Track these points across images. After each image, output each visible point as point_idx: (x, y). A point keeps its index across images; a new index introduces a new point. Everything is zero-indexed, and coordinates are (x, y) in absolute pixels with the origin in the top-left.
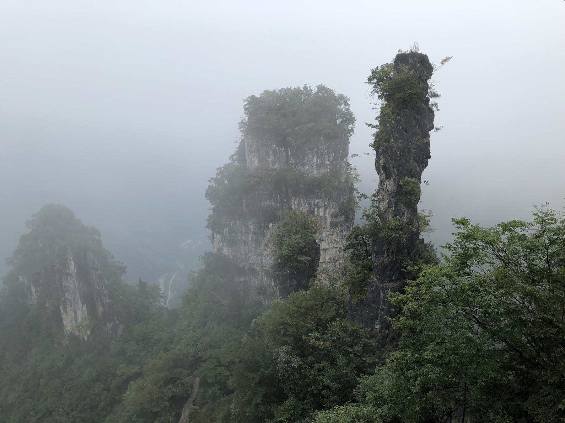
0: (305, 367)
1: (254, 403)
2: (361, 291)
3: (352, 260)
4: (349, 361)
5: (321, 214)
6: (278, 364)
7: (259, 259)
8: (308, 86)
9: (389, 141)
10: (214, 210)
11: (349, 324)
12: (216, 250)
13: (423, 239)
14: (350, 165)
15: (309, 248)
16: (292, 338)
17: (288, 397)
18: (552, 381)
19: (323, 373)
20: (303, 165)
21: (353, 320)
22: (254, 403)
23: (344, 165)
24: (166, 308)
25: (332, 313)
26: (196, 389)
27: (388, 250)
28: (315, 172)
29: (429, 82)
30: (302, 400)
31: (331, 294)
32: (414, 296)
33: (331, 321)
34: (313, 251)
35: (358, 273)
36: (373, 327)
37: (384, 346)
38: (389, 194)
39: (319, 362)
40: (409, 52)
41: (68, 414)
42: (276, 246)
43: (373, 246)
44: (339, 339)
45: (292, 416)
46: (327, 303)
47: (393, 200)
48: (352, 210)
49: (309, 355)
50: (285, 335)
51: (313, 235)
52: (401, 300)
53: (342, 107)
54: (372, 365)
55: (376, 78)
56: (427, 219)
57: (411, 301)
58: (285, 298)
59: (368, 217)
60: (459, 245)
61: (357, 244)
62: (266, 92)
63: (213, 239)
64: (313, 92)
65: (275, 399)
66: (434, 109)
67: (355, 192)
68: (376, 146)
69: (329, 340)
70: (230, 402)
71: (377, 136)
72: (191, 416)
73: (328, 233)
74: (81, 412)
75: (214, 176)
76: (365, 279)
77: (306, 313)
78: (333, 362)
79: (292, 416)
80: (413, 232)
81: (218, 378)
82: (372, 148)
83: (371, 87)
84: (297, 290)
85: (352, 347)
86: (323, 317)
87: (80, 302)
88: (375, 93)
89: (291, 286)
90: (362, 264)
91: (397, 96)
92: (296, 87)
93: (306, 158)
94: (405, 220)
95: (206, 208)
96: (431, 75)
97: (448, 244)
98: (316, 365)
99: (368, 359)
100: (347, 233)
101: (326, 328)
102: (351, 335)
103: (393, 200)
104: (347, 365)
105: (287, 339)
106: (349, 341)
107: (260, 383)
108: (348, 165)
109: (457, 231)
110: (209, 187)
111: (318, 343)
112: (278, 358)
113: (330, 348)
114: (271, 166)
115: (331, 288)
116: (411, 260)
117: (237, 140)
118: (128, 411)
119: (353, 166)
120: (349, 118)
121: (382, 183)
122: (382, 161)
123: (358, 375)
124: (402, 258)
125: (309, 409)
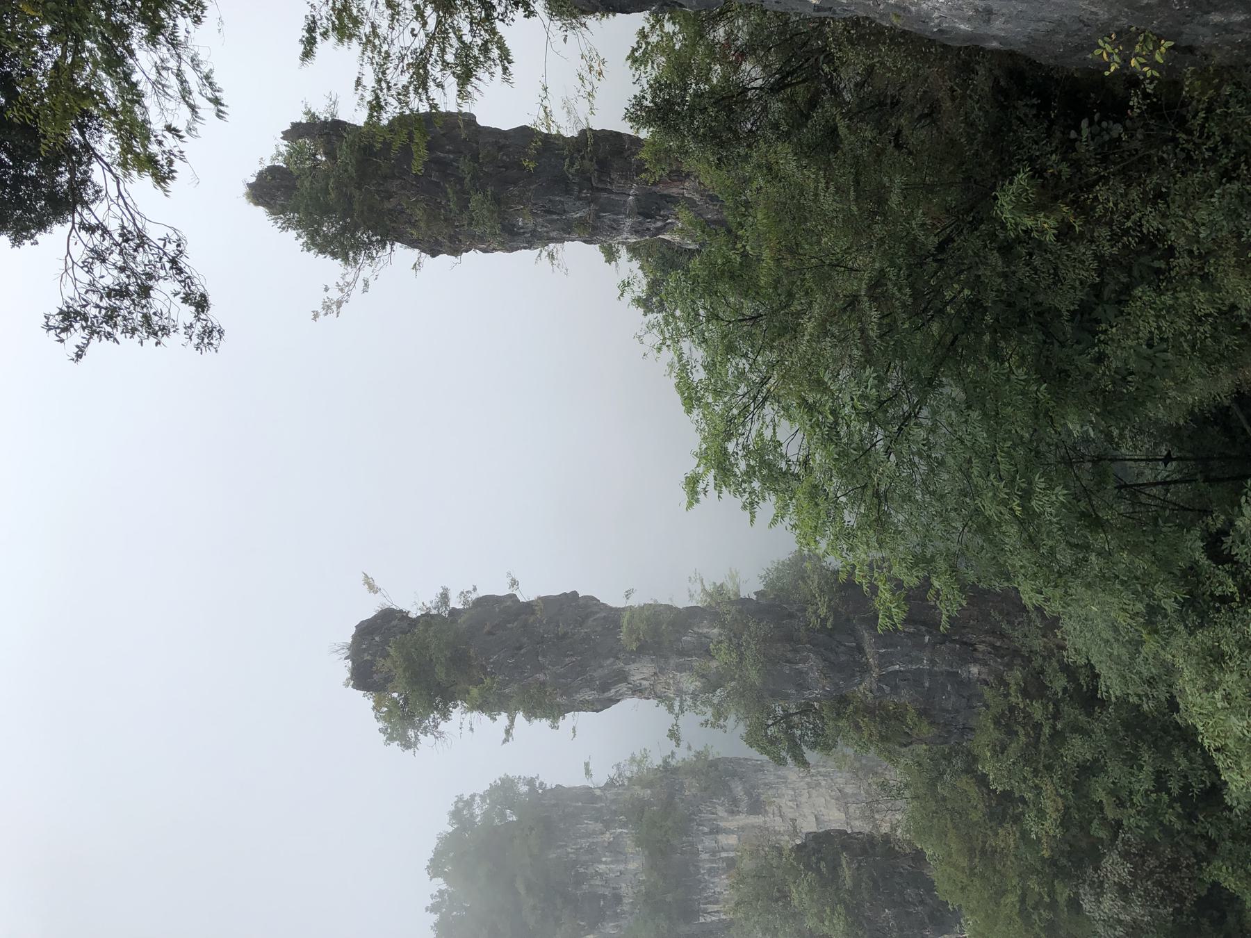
0: (1125, 842)
2: (899, 716)
3: (827, 748)
4: (1077, 729)
5: (732, 840)
8: (429, 902)
9: (543, 684)
11: (984, 739)
13: (756, 593)
14: (612, 780)
15: (819, 860)
17: (1216, 885)
18: (1000, 263)
20: (618, 899)
21: (972, 730)
23: (610, 795)
25: (965, 782)
27: (788, 661)
28: (632, 866)
29: (414, 613)
30: (1212, 845)
31: (922, 791)
32: (878, 567)
33: (987, 786)
34: (821, 850)
35: (858, 728)
36: (978, 680)
37: (1016, 653)
38: (662, 671)
40: (349, 663)
43: (786, 697)
44: (1027, 762)
46: (944, 799)
47: (674, 661)
48: (714, 764)
50: (1053, 905)
51: (786, 852)
52: (893, 595)
53: (478, 812)
54: (1069, 670)
56: (709, 588)
57: (890, 568)
59: (719, 715)
60: (744, 485)
61: (785, 738)
64: (444, 887)
65: (1231, 919)
66: (474, 596)
67: (673, 763)
68: (554, 712)
69: (1037, 787)
71: (531, 714)
73: (778, 819)
76: (870, 711)
77: (983, 852)
78: (1088, 770)
80: (740, 612)
82: (561, 722)
83: (426, 740)
84: (930, 886)
85: (1038, 726)
88: (440, 728)
89: (922, 902)
90: (835, 720)
91: (443, 675)
93: (601, 891)
94: (716, 631)
96: (401, 611)
97: (744, 508)
98: (1110, 813)
100: (771, 772)
101: (1007, 796)
102: (1012, 733)
103: (674, 661)
104: (1085, 733)
106: (1027, 735)
108: (611, 784)
109: (713, 493)
111: (1052, 815)
112: (1120, 922)
115: (907, 793)
119: (613, 773)
120: (504, 792)
121: (637, 691)
122: (588, 695)
123: (1104, 704)
124: (802, 629)
125: (1229, 821)
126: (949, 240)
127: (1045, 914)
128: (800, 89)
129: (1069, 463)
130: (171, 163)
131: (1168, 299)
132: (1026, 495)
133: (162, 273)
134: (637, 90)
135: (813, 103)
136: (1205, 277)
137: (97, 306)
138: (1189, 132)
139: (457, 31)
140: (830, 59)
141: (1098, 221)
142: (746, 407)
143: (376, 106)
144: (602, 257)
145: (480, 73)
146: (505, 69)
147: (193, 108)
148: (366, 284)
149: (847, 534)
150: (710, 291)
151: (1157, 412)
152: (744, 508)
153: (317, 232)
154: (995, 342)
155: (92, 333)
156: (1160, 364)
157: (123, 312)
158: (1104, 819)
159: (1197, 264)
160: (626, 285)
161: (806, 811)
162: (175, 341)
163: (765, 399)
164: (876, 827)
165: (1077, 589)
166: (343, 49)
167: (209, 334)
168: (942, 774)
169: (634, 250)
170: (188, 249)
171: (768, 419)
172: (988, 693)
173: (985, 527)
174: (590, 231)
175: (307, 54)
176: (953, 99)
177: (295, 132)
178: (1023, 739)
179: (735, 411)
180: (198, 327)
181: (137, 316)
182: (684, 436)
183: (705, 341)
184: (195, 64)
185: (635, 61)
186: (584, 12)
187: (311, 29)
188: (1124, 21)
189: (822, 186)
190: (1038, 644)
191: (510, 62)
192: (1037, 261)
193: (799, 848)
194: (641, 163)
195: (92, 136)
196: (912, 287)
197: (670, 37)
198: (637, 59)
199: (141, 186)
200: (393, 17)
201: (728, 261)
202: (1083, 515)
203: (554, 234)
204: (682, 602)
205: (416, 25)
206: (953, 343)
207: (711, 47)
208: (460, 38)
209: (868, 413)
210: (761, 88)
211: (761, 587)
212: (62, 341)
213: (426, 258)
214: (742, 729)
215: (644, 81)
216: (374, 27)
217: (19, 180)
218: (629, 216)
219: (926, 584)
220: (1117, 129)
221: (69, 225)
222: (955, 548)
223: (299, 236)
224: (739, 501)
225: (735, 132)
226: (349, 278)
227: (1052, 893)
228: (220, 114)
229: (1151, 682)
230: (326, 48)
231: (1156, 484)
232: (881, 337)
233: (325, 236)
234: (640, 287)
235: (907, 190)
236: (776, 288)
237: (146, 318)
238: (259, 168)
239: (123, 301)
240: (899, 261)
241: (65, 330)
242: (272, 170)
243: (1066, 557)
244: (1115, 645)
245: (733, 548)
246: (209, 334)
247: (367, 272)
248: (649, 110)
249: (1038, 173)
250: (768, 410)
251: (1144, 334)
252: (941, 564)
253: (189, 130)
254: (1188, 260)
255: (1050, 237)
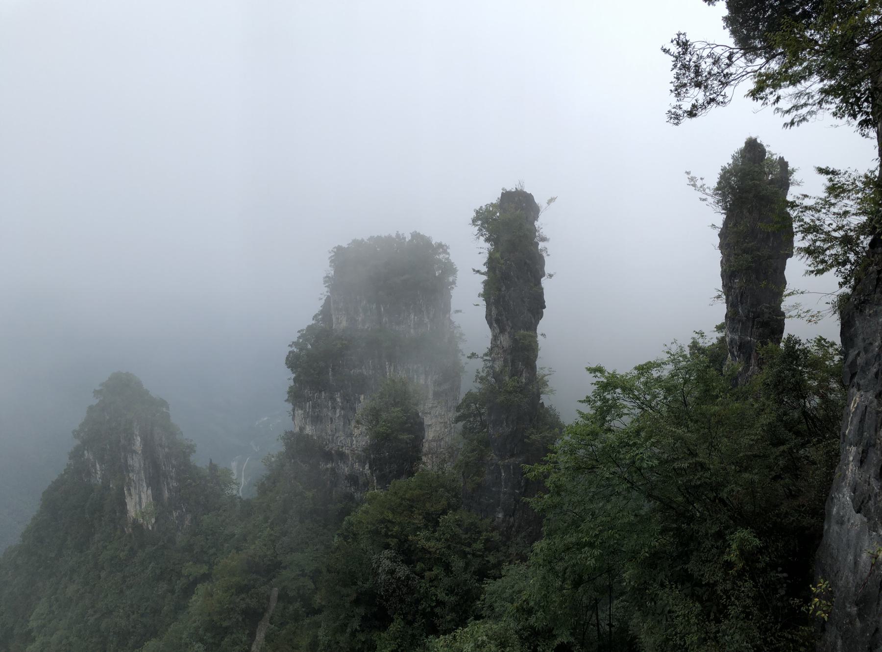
1: (349, 630)
4: (467, 565)
6: (378, 574)
7: (349, 440)
8: (400, 233)
10: (295, 380)
12: (297, 429)
16: (395, 540)
17: (392, 620)
19: (435, 583)
22: (349, 630)
24: (240, 498)
25: (444, 502)
26: (273, 604)
28: (412, 331)
29: (537, 224)
30: (410, 623)
33: (441, 514)
35: (473, 451)
38: (504, 351)
39: (431, 570)
41: (129, 616)
42: (371, 422)
45: (400, 646)
46: (437, 491)
49: (418, 561)
53: (441, 256)
55: (480, 219)
56: (546, 378)
57: (555, 472)
58: (384, 488)
59: (482, 379)
62: (354, 241)
63: (294, 415)
64: (407, 240)
66: (544, 254)
70: (318, 625)
71: (486, 284)
72: (268, 638)
73: (430, 405)
74: (142, 615)
75: (295, 340)
77: (412, 507)
78: (447, 568)
79: (400, 646)
81: (301, 592)
84: (398, 476)
85: (469, 545)
86: (433, 509)
87: (144, 484)
92: (387, 234)
95: (286, 378)
97: (587, 397)
98: (427, 574)
99: (492, 559)
102: (467, 531)
104: (466, 569)
105: (389, 540)
107: (357, 602)
108: (451, 322)
109: (595, 380)
110: (290, 352)
111: (428, 545)
112: (379, 567)
113: (443, 550)
114: (360, 326)
116: (534, 427)
117: (322, 296)
118: (195, 622)
119: (456, 324)
120: (449, 269)
121: (495, 338)
122: (494, 312)
123: (480, 580)
125: (421, 635)
126: (725, 505)
127: (383, 531)
128: (805, 427)
129: (609, 571)
130: (761, 99)
131: (693, 620)
132: (591, 545)
133: (708, 94)
134: (803, 341)
135: (798, 434)
136: (705, 640)
137: (690, 60)
138: (781, 630)
139: (832, 247)
140: (819, 442)
141: (734, 583)
142: (639, 399)
143: (793, 205)
144: (719, 323)
145: (810, 261)
146: (812, 272)
147: (788, 111)
148: (704, 200)
149: (572, 451)
150: (699, 379)
151: (636, 618)
152: (587, 397)
153: (732, 174)
154: (671, 530)
155: (676, 57)
156: (659, 618)
157: (687, 73)
158: (425, 571)
159: (712, 636)
160: (702, 334)
161: (434, 420)
162: (673, 100)
163: (643, 409)
164: (425, 455)
165: (541, 572)
166: (823, 188)
167: (676, 118)
168: (448, 492)
169: (722, 340)
170: (720, 108)
171: (632, 411)
172: (488, 521)
173: (575, 525)
174: (732, 317)
175: (821, 171)
176: (799, 506)
177: (783, 163)
178: (463, 536)
179: (636, 393)
180: (680, 112)
181: (685, 81)
182: (623, 365)
183: (673, 377)
184: (811, 113)
185: (819, 340)
186: (841, 313)
187: (834, 173)
188: (837, 594)
189: (753, 437)
190: (513, 550)
191: (816, 274)
192: (714, 551)
193: (417, 414)
194: (766, 344)
195: (779, 59)
196: (700, 485)
197: (832, 359)
198: (820, 341)
199: (750, 84)
200: (838, 214)
201: (714, 388)
202: (580, 577)
203: (730, 298)
204: (539, 363)
205: (834, 226)
206: (671, 507)
207: (826, 380)
208: (828, 249)
209: (634, 462)
210: (805, 406)
211: (546, 406)
212: (672, 41)
213: (718, 231)
214: (475, 390)
215: (808, 345)
216: (834, 204)
217: (758, 21)
218: (740, 337)
219: (547, 491)
220: (782, 592)
221: (733, 46)
222: (565, 508)
223: (729, 165)
224: (590, 394)
225: (782, 392)
226: (707, 191)
227: (392, 536)
228: (786, 125)
229: (491, 607)
230: (824, 179)
231: (597, 619)
232: (674, 469)
233: (729, 179)
234: (701, 342)
235: (752, 482)
236: (701, 414)
237: (685, 85)
238: (765, 145)
239: (693, 75)
240: (714, 478)
241: (678, 44)
242: (763, 152)
243: (559, 567)
244: (511, 591)
245: (567, 393)
246: (676, 118)
247: (711, 200)
248: (793, 347)
249: (760, 551)
250: (638, 411)
251: (675, 608)
252: (556, 499)
253: (778, 109)
254: (714, 631)
255: (726, 557)
